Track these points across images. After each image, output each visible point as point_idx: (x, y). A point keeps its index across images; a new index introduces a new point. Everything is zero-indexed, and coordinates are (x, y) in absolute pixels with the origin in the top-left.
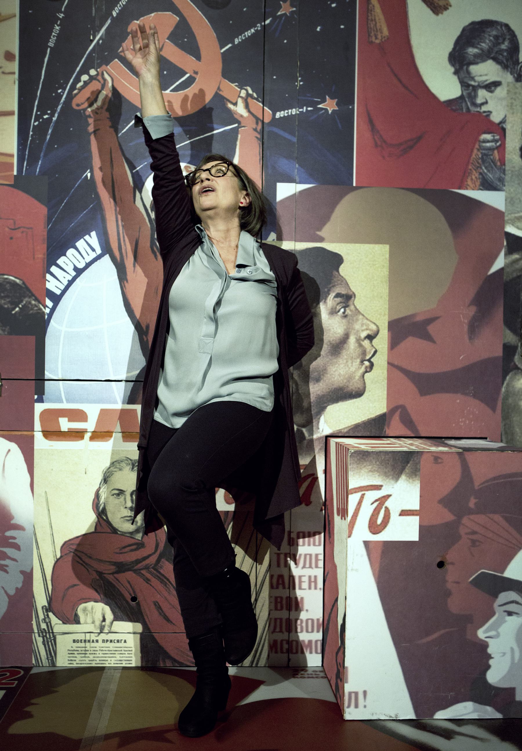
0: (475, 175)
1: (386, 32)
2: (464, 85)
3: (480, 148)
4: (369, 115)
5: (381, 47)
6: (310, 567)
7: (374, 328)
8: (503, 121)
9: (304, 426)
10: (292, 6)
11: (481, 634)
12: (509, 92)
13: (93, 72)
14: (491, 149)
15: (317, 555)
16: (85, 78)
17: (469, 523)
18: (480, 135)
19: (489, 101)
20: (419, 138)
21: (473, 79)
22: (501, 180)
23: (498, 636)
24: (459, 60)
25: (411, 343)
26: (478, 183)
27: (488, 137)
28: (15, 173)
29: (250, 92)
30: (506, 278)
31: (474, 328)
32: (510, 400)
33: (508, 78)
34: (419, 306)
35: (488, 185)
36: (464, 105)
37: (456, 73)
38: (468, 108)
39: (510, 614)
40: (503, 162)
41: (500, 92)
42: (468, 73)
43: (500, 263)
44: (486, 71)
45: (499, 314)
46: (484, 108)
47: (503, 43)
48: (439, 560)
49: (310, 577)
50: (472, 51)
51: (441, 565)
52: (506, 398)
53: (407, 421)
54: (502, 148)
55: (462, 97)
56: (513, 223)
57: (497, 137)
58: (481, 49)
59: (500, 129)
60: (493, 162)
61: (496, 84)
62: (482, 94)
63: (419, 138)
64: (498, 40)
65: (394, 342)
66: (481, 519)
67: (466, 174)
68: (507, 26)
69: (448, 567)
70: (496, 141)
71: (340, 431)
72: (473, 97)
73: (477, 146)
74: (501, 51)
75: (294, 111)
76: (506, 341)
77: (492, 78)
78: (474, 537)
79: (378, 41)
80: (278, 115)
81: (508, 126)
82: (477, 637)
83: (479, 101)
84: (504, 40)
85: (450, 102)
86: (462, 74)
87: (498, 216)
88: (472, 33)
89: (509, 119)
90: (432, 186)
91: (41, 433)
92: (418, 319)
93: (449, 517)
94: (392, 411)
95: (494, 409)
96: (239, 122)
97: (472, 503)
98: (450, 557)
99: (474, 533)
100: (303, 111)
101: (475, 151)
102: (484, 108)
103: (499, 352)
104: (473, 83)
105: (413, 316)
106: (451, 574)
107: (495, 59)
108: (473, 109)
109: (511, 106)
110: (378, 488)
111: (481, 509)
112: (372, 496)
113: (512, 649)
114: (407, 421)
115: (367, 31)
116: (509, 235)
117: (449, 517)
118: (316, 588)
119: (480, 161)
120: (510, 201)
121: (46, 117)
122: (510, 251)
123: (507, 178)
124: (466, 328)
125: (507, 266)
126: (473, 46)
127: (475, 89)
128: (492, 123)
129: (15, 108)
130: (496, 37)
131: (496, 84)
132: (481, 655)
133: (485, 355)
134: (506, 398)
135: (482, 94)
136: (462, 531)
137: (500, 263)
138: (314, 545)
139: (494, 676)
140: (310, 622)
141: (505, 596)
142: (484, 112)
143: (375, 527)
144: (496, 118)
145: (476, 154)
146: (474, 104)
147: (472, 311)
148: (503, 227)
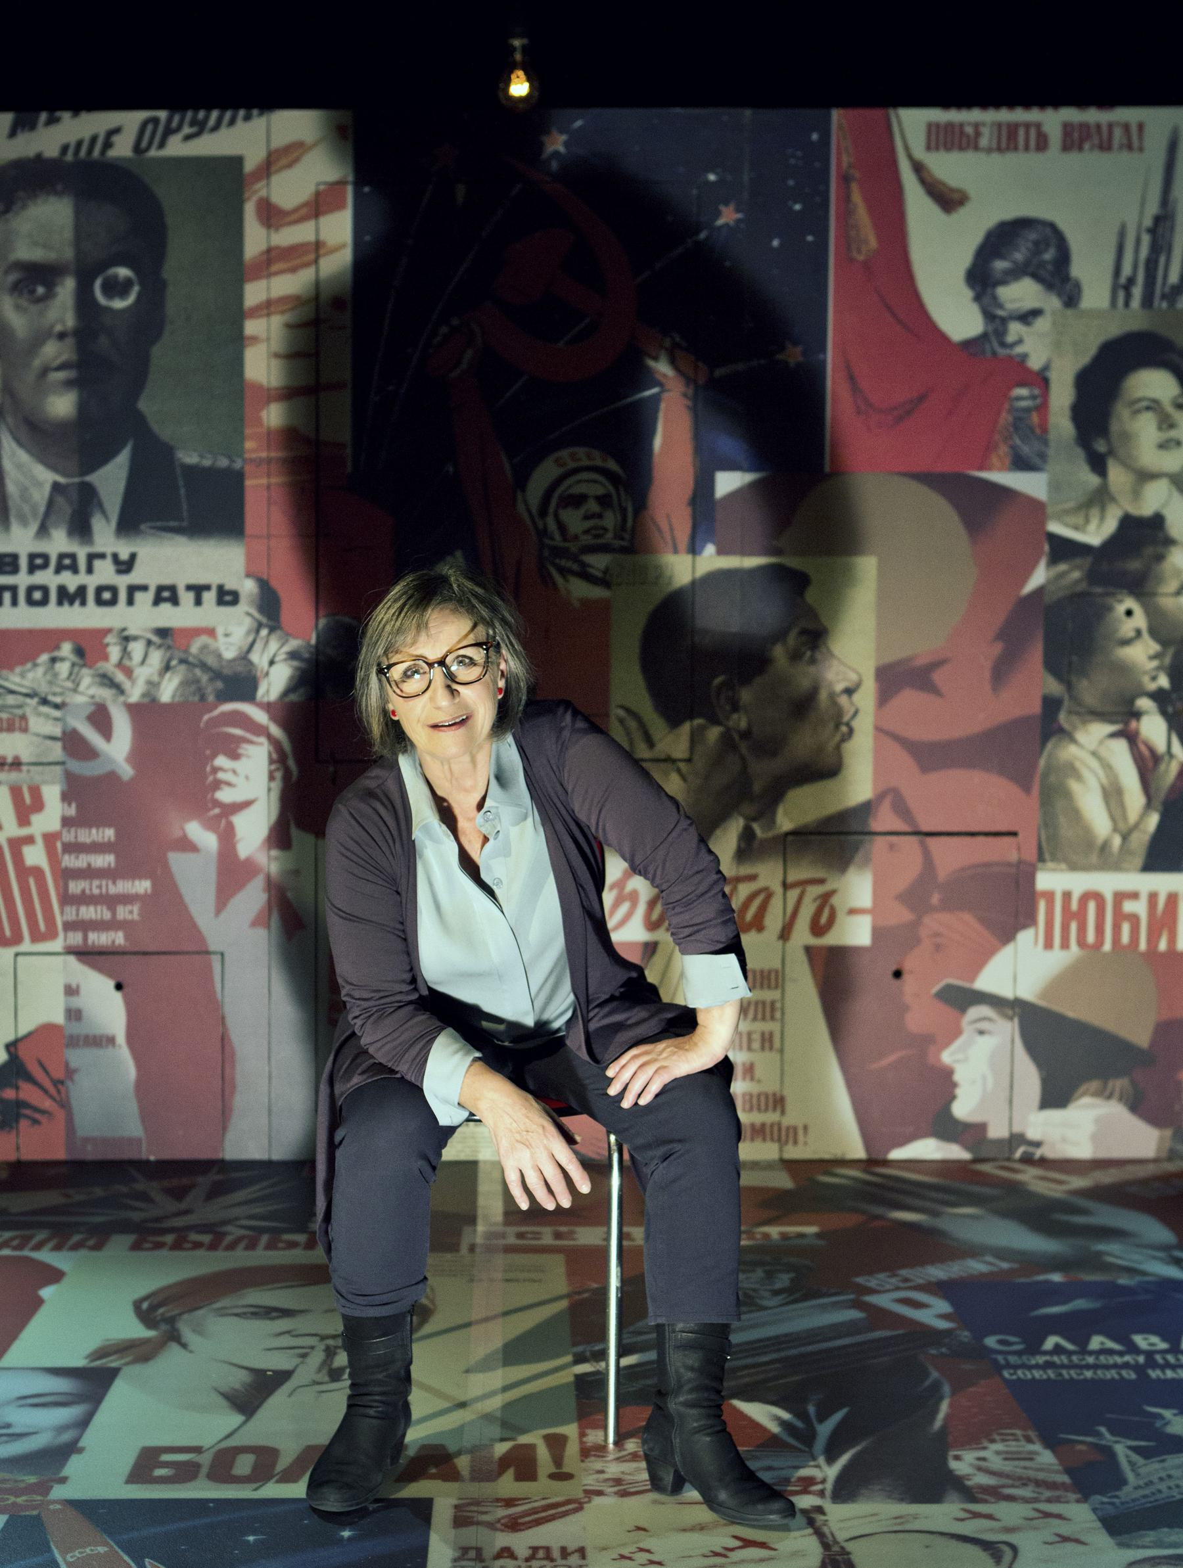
0: (1003, 449)
1: (873, 243)
2: (989, 316)
3: (1012, 410)
4: (848, 368)
5: (867, 266)
6: (764, 1019)
7: (854, 677)
8: (1046, 368)
9: (754, 819)
10: (737, 211)
11: (947, 1057)
12: (1054, 323)
13: (455, 322)
14: (1028, 410)
15: (773, 1003)
16: (444, 329)
17: (932, 923)
18: (1010, 388)
19: (1026, 338)
20: (922, 398)
21: (1001, 306)
22: (1043, 456)
23: (966, 1060)
24: (981, 279)
25: (908, 698)
26: (1008, 461)
27: (1023, 392)
28: (349, 469)
29: (678, 339)
30: (1048, 599)
31: (1001, 672)
32: (1052, 779)
33: (1052, 303)
34: (919, 646)
35: (1021, 464)
36: (987, 346)
37: (977, 298)
38: (994, 353)
39: (981, 1033)
40: (1044, 428)
41: (1042, 324)
42: (995, 298)
43: (1039, 577)
44: (1021, 293)
45: (1036, 654)
46: (1019, 350)
47: (1046, 250)
48: (894, 968)
49: (763, 1034)
50: (1000, 265)
51: (898, 974)
52: (1046, 775)
53: (901, 808)
54: (1043, 408)
55: (985, 336)
56: (1059, 517)
57: (1037, 392)
58: (1014, 262)
59: (1041, 380)
60: (1032, 430)
61: (1036, 313)
62: (1015, 329)
63: (922, 398)
64: (1038, 248)
65: (884, 696)
66: (945, 917)
67: (989, 448)
68: (1052, 226)
69: (906, 977)
70: (1033, 397)
71: (805, 826)
72: (1001, 333)
73: (1007, 406)
74: (1042, 264)
75: (740, 367)
76: (1047, 691)
77: (1028, 304)
78: (938, 940)
79: (861, 258)
80: (718, 373)
81: (1053, 376)
82: (939, 1060)
83: (1010, 339)
84: (1048, 245)
85: (967, 344)
86: (986, 300)
87: (1036, 509)
88: (1001, 238)
89: (1056, 365)
90: (940, 468)
91: (212, 948)
92: (920, 662)
93: (907, 916)
94: (880, 797)
95: (1027, 789)
96: (661, 385)
97: (935, 899)
98: (907, 966)
99: (937, 935)
100: (421, 997)
101: (1004, 414)
102: (1019, 350)
103: (1036, 708)
104: (1000, 313)
105: (909, 659)
106: (909, 983)
107: (1036, 277)
108: (1002, 352)
109: (1057, 345)
110: (821, 881)
111: (947, 906)
112: (814, 891)
113: (984, 1078)
114: (901, 808)
115: (847, 242)
116: (1053, 538)
117: (907, 916)
118: (771, 1048)
119: (1011, 429)
120: (1055, 486)
121: (391, 388)
122: (1054, 560)
123: (1051, 452)
124: (987, 674)
125: (1049, 582)
126: (1001, 257)
127: (1004, 321)
128: (1028, 371)
129: (347, 376)
130: (1036, 244)
131: (1036, 313)
132: (945, 1083)
133: (1017, 712)
134: (1046, 775)
135: (1015, 329)
136: (923, 932)
137: (1039, 577)
138: (769, 987)
139: (962, 1109)
140: (763, 1099)
141: (975, 1012)
142: (1019, 355)
143: (818, 929)
144: (1035, 363)
145: (1005, 418)
146: (1003, 344)
147: (998, 648)
148: (1043, 523)
